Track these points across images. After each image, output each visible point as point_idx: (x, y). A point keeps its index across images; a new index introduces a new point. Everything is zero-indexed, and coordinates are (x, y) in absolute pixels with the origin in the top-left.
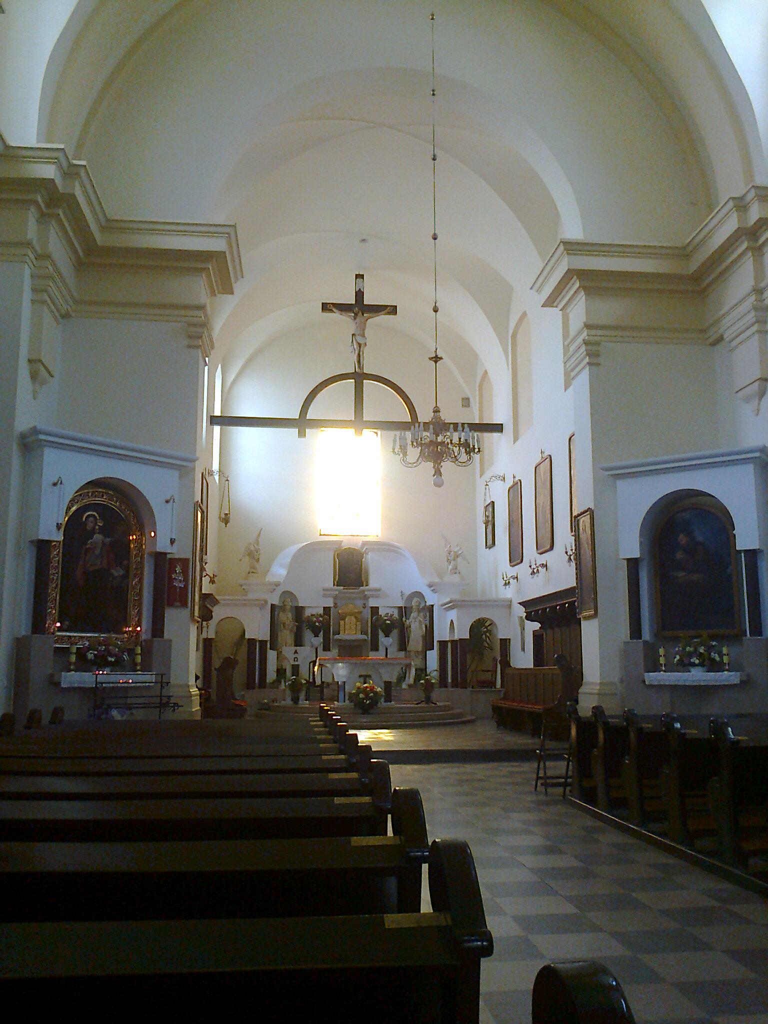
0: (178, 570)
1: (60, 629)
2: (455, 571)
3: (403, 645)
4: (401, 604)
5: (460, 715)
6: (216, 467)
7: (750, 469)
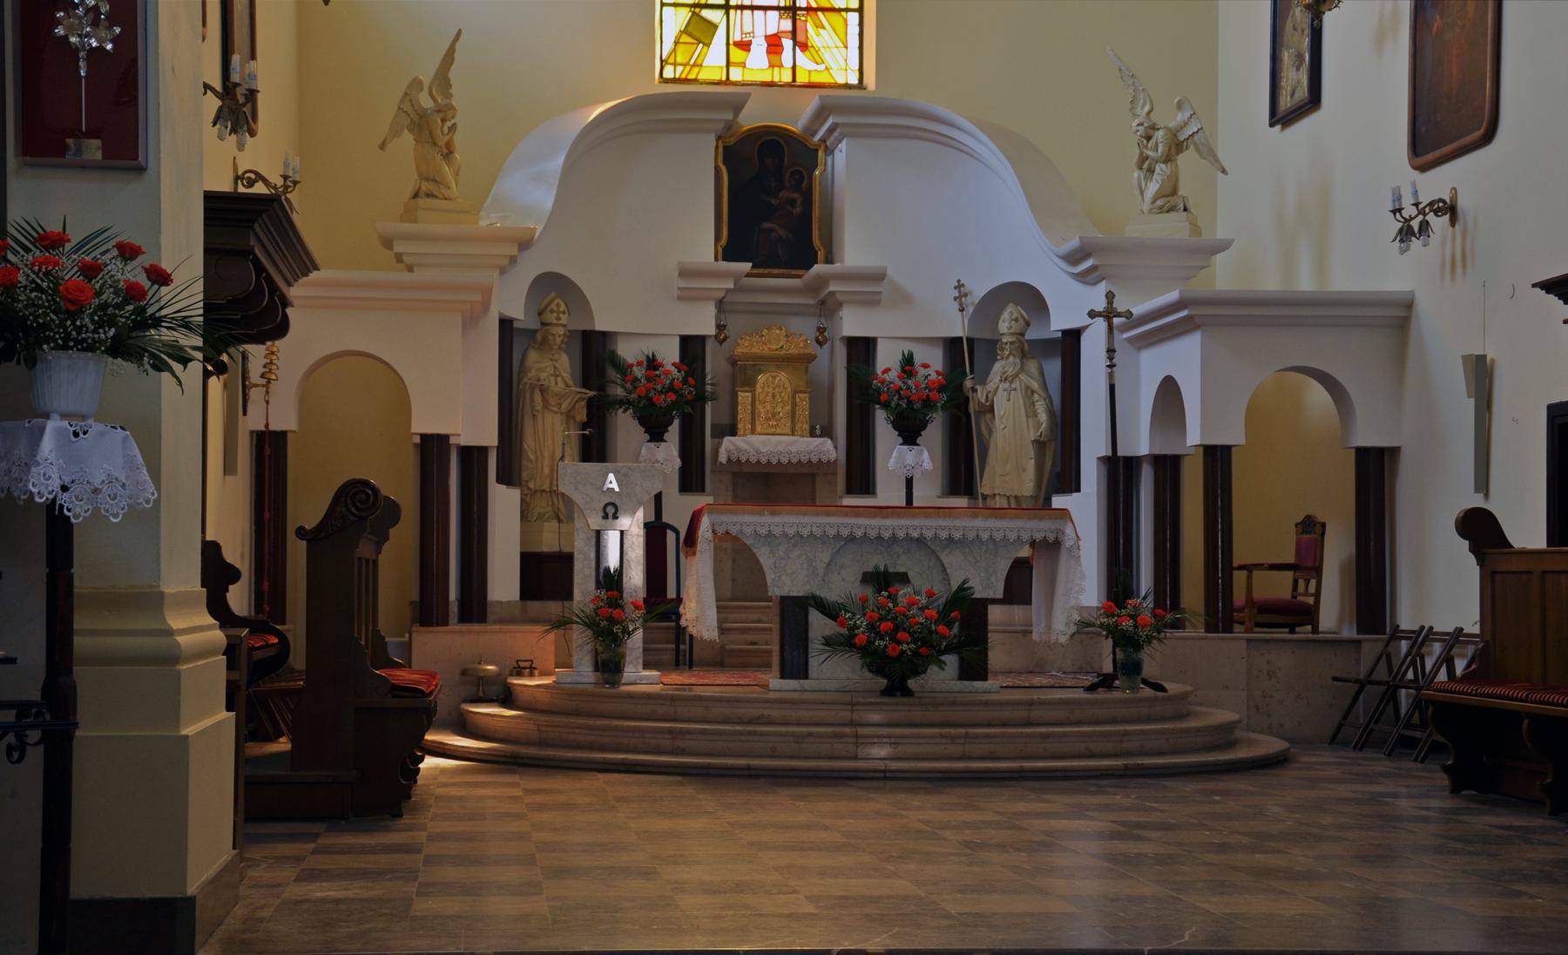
2: (1170, 200)
3: (962, 473)
4: (957, 327)
5: (1224, 736)
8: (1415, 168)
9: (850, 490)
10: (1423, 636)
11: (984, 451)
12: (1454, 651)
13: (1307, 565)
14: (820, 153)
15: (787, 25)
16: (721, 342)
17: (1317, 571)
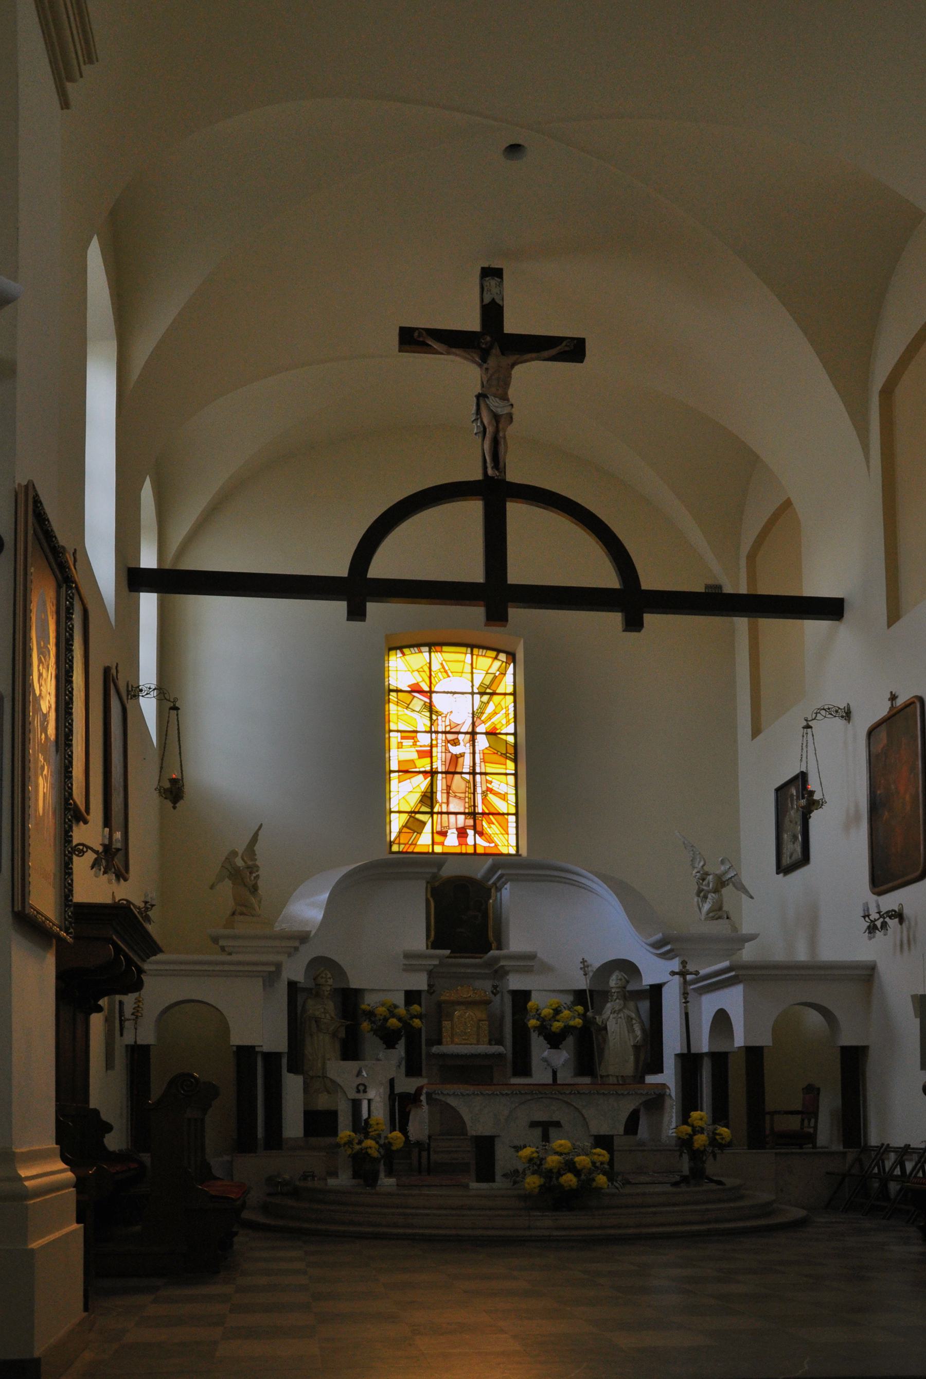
2: (718, 913)
4: (582, 984)
6: (148, 674)
8: (874, 893)
9: (516, 1074)
10: (885, 1149)
11: (602, 1051)
12: (905, 1157)
13: (810, 1112)
14: (493, 891)
15: (471, 822)
16: (431, 994)
17: (815, 1114)
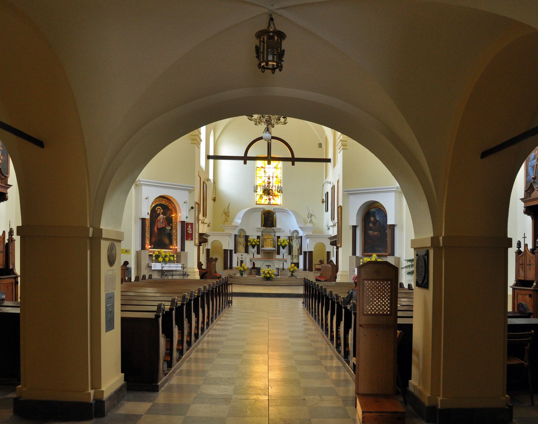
0: (190, 227)
1: (150, 248)
2: (311, 222)
3: (290, 253)
4: (290, 235)
6: (211, 177)
7: (393, 194)
